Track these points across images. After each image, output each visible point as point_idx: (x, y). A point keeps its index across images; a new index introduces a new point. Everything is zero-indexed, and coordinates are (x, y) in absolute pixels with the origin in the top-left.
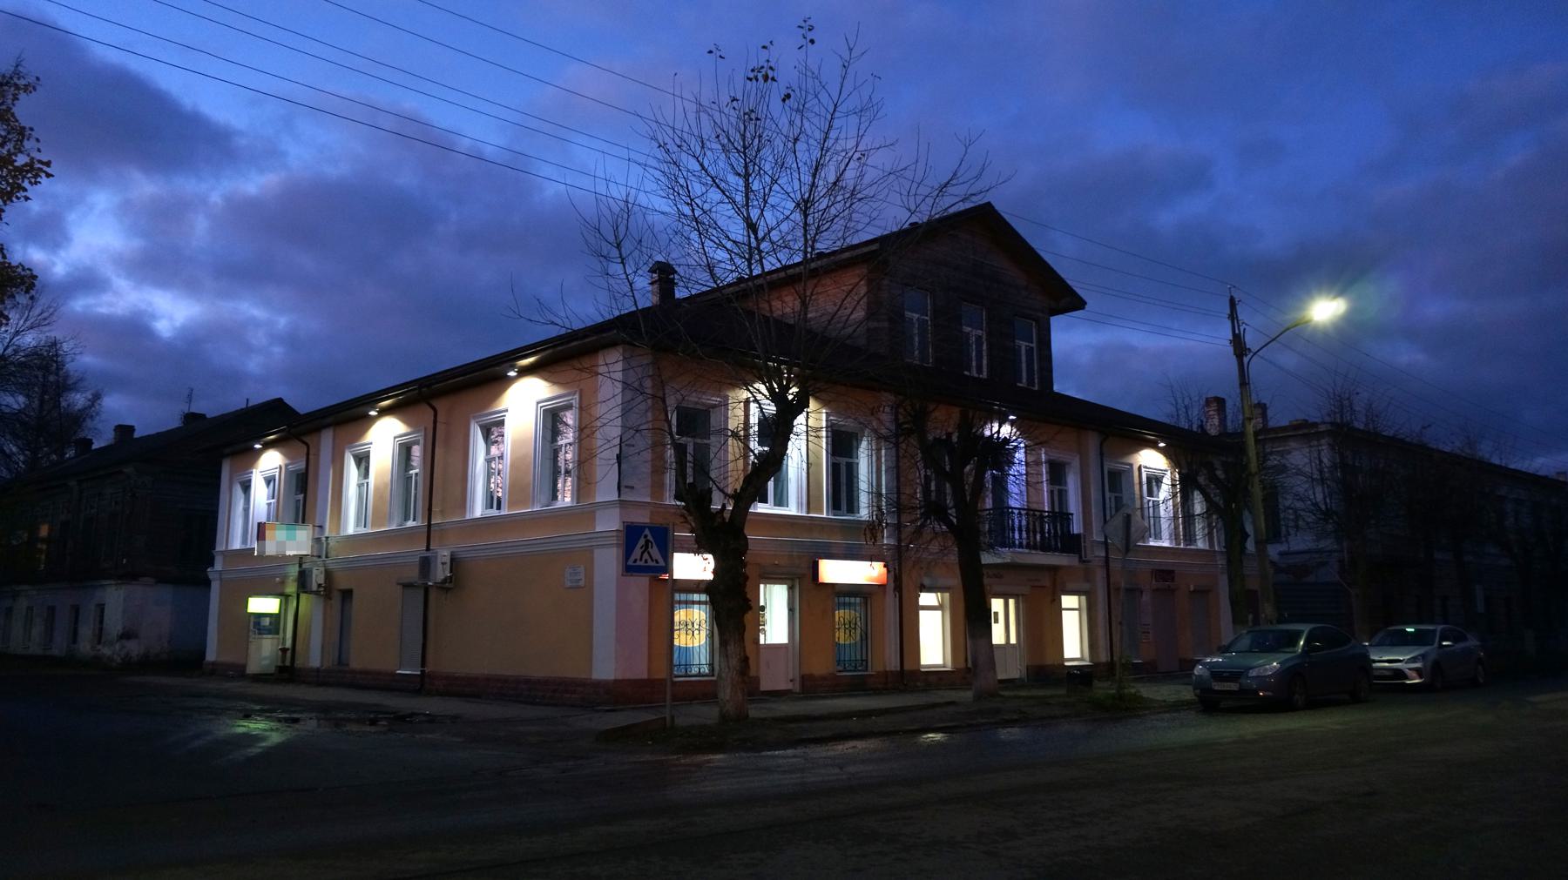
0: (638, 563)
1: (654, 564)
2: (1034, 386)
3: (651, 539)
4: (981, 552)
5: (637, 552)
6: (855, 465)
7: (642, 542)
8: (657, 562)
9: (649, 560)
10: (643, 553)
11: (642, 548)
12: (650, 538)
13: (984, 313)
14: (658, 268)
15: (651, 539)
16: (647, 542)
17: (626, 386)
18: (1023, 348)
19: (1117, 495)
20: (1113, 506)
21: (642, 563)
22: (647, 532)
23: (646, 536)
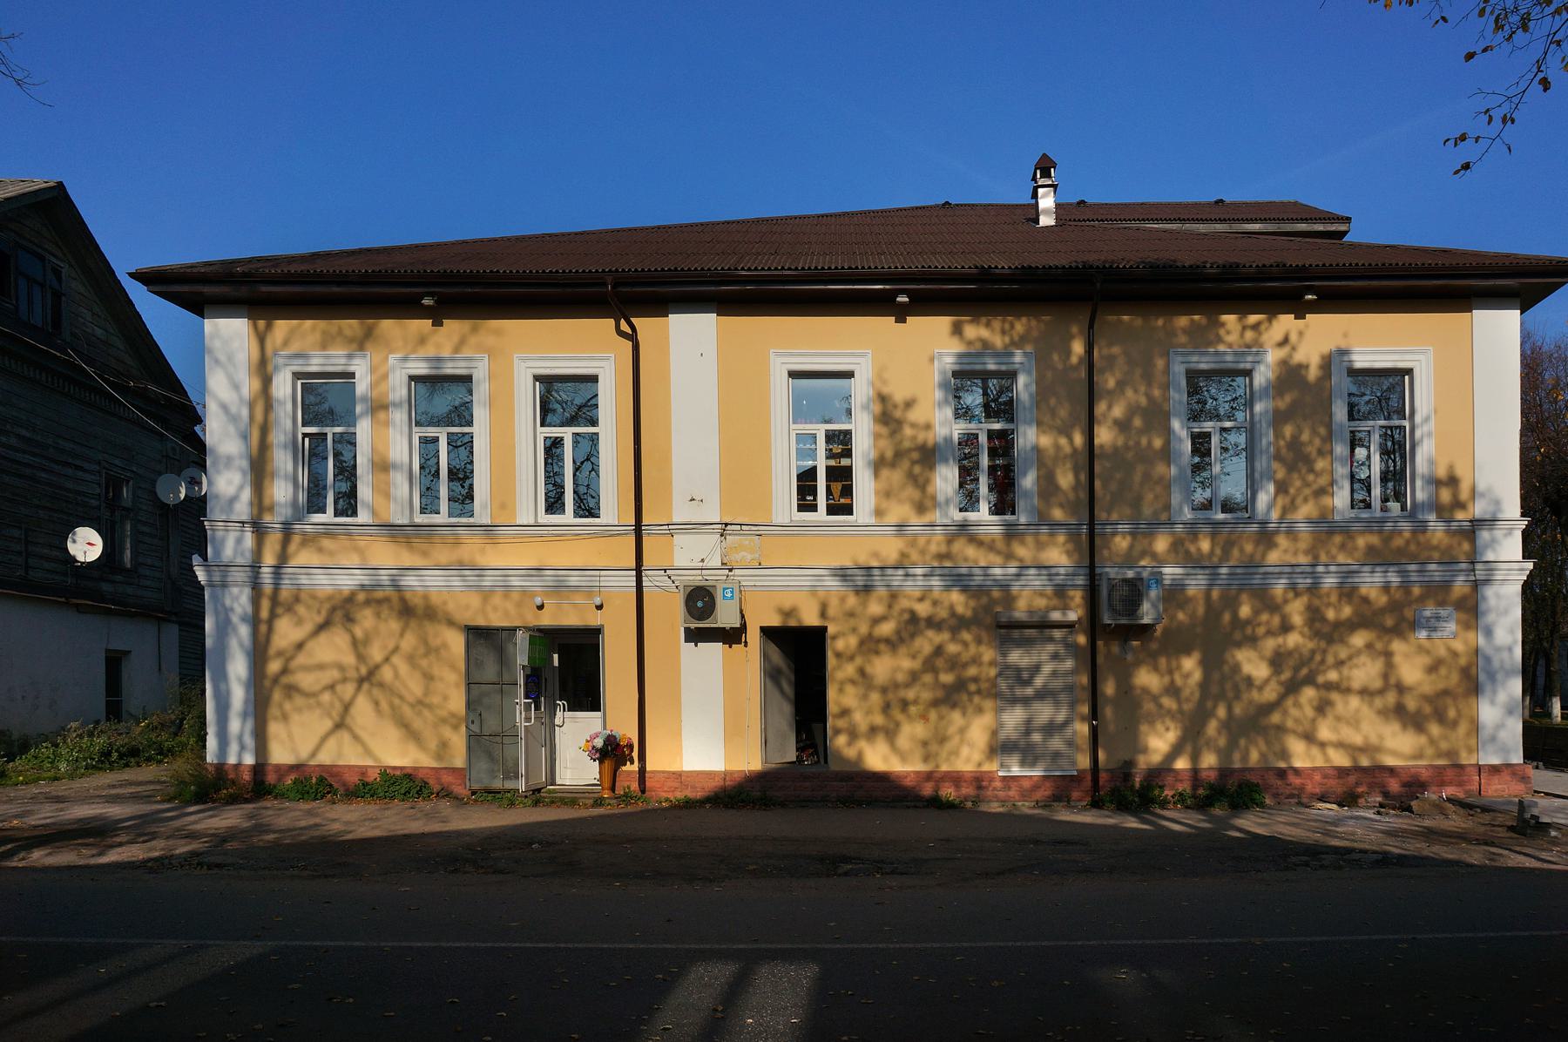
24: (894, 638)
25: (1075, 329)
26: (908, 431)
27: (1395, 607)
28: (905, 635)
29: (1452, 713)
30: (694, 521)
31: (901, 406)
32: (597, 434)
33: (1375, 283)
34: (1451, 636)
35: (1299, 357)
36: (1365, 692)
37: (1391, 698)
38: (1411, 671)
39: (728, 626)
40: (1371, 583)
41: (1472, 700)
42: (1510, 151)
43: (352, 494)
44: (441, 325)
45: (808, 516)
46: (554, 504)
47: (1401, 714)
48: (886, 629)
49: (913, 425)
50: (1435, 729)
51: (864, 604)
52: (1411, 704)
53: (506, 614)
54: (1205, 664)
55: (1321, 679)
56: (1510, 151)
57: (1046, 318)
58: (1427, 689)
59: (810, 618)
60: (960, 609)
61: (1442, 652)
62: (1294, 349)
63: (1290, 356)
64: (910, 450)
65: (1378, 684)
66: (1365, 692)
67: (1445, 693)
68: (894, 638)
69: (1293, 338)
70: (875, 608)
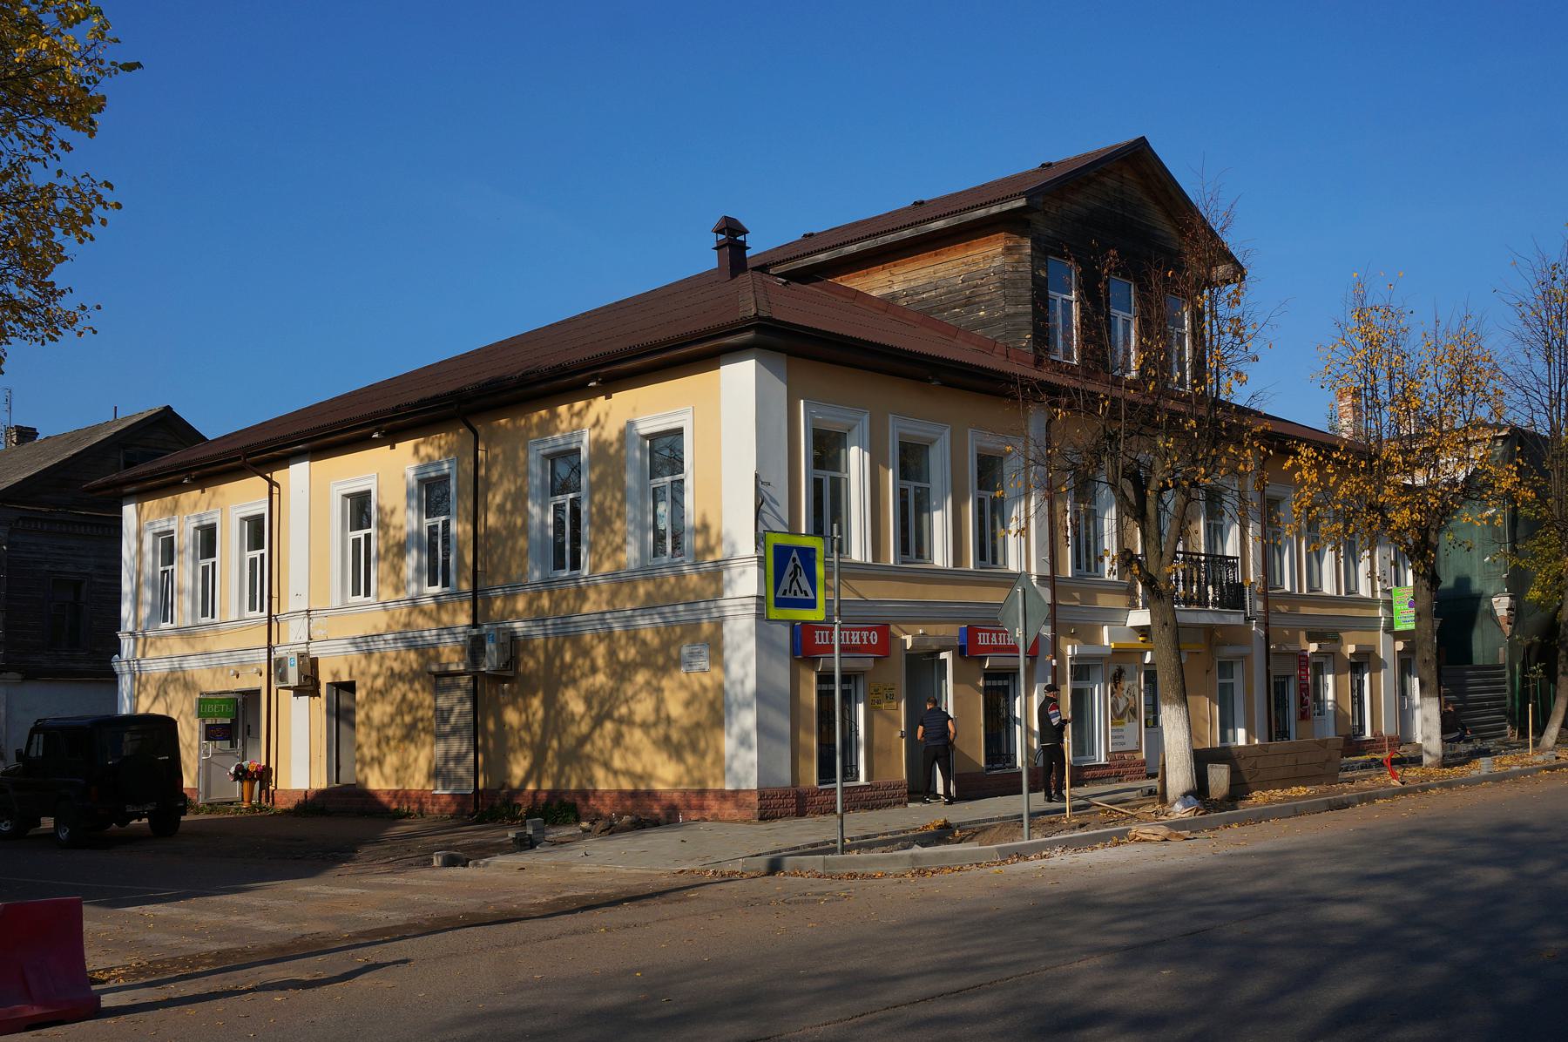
0: (788, 595)
1: (802, 596)
2: (1072, 359)
3: (800, 565)
4: (283, 804)
5: (786, 579)
6: (843, 481)
7: (790, 567)
8: (806, 595)
9: (798, 592)
10: (792, 581)
11: (790, 576)
12: (798, 562)
13: (1330, 695)
14: (727, 228)
15: (800, 565)
16: (796, 567)
17: (1406, 751)
18: (1059, 301)
19: (918, 484)
20: (1557, 382)
21: (791, 596)
22: (795, 554)
23: (794, 560)
24: (383, 689)
26: (392, 532)
27: (665, 646)
29: (702, 744)
31: (389, 513)
34: (701, 675)
35: (605, 435)
36: (645, 726)
41: (717, 731)
45: (358, 599)
52: (675, 735)
58: (686, 722)
60: (415, 666)
63: (600, 435)
65: (652, 718)
66: (645, 726)
67: (698, 725)
69: (602, 418)
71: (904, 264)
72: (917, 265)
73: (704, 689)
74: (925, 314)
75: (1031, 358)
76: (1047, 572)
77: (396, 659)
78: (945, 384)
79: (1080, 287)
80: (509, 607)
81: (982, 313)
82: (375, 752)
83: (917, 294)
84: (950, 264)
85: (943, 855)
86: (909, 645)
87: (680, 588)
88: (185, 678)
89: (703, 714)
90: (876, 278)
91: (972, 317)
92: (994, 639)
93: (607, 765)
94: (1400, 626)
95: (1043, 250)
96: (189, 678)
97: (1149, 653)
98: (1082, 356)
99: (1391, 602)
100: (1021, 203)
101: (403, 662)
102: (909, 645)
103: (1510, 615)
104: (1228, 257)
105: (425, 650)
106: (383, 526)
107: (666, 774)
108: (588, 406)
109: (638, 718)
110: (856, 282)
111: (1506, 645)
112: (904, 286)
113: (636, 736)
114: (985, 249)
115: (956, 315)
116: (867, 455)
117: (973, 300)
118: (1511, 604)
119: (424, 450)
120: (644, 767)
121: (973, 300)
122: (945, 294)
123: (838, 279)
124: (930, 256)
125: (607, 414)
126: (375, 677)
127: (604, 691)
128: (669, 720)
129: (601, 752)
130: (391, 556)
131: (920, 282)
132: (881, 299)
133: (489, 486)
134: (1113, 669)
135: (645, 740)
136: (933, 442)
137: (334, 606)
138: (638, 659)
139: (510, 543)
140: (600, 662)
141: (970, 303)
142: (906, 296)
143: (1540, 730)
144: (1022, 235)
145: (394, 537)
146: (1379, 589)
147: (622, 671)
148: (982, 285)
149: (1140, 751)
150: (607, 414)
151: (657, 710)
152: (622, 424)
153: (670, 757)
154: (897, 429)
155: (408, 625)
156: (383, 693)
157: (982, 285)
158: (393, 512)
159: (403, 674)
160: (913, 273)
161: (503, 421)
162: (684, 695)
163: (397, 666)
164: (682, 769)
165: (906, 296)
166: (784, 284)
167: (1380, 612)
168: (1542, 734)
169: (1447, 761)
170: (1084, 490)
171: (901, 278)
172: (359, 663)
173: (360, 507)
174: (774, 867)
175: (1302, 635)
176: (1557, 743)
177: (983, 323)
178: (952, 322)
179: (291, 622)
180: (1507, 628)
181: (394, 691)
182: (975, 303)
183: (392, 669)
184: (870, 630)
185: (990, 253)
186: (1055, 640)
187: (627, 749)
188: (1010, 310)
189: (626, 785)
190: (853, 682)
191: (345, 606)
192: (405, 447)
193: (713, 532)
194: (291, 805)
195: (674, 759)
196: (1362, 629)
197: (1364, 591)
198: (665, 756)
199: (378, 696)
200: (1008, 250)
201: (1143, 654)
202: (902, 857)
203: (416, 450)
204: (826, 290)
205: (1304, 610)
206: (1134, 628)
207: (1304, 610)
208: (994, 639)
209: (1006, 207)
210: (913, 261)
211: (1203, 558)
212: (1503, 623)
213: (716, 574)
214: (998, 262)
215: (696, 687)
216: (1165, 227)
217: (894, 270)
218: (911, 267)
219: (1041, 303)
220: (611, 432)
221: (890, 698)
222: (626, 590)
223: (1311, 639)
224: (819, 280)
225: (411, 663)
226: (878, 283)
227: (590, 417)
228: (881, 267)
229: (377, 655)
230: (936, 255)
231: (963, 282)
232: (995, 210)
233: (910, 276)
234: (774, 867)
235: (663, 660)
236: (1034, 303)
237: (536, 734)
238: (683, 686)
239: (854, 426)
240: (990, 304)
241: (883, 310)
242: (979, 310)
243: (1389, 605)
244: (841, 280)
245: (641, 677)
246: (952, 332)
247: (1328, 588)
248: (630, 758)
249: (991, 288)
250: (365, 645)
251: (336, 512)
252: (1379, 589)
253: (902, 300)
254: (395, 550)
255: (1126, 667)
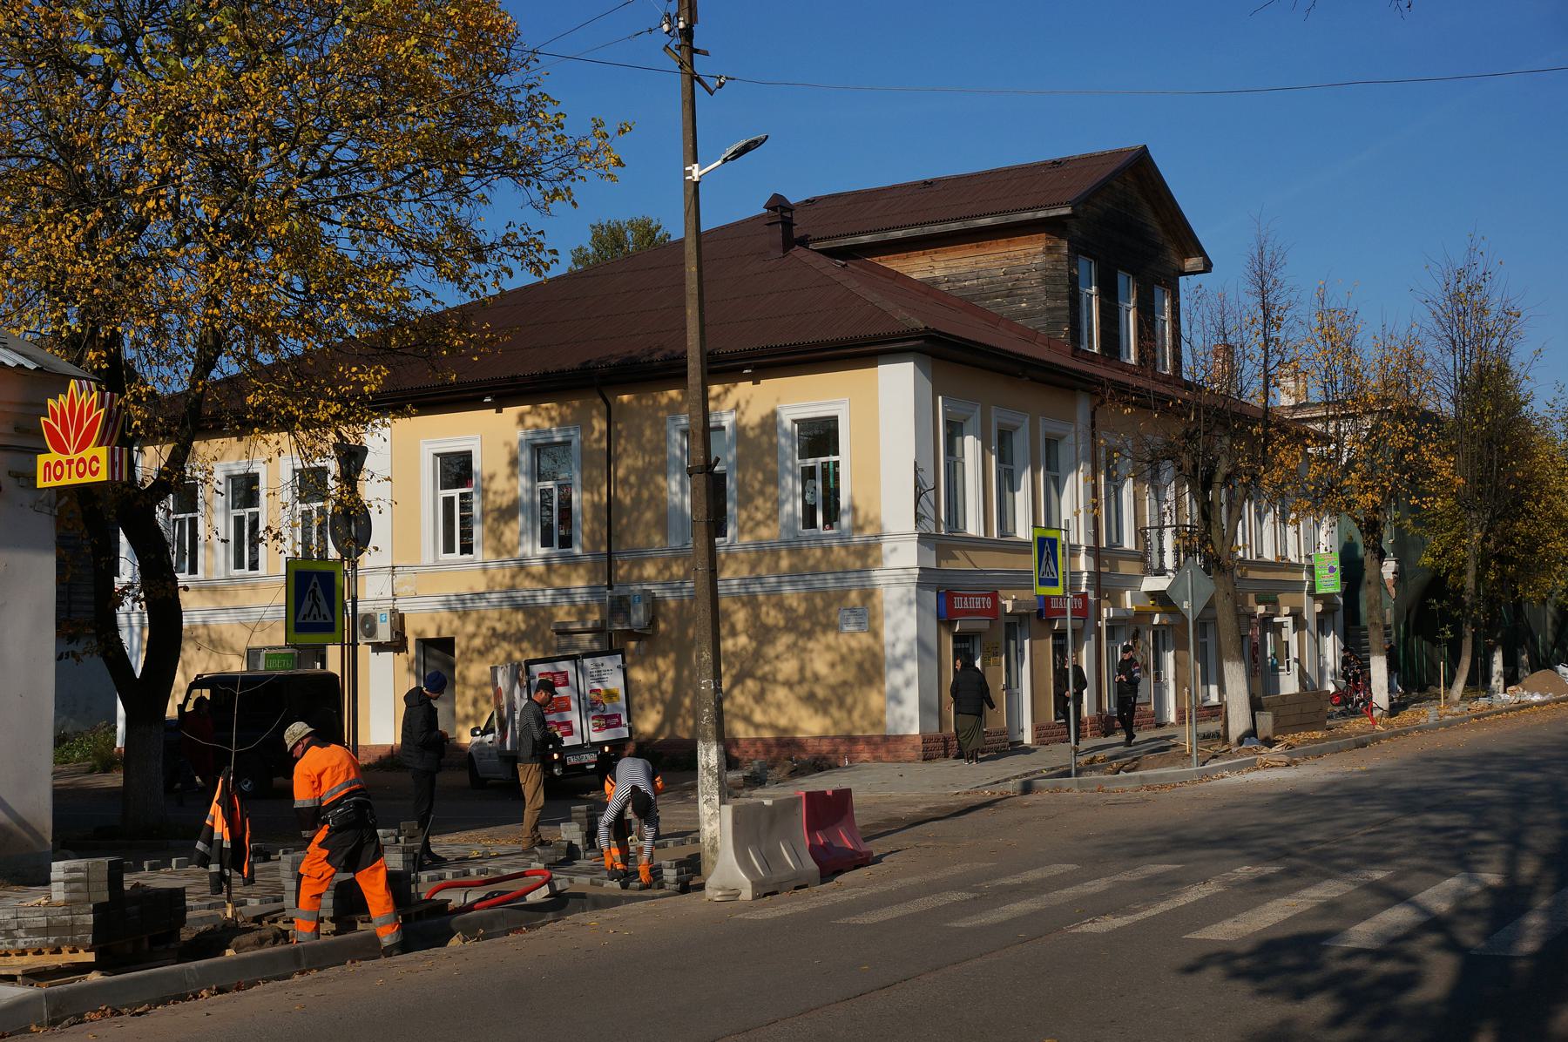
5: (1044, 563)
18: (1084, 295)
24: (483, 648)
25: (595, 412)
26: (491, 496)
27: (811, 613)
28: (513, 639)
29: (849, 700)
30: (375, 565)
31: (487, 478)
32: (258, 513)
33: (808, 355)
34: (852, 639)
35: (744, 421)
36: (788, 684)
37: (803, 690)
38: (820, 665)
39: (383, 641)
40: (792, 595)
41: (865, 689)
42: (755, 144)
43: (467, 533)
44: (242, 440)
45: (449, 556)
46: (449, 548)
47: (810, 699)
48: (477, 642)
49: (495, 493)
50: (834, 711)
51: (464, 624)
52: (821, 692)
53: (262, 642)
54: (679, 665)
55: (759, 673)
56: (755, 144)
57: (576, 403)
58: (832, 680)
59: (445, 633)
60: (523, 626)
61: (844, 650)
62: (743, 413)
63: (740, 419)
64: (492, 511)
65: (796, 677)
66: (788, 684)
67: (845, 683)
68: (483, 648)
69: (743, 405)
70: (470, 628)
71: (945, 252)
72: (959, 254)
73: (851, 650)
74: (966, 303)
75: (1069, 348)
76: (1091, 544)
77: (500, 620)
78: (1033, 379)
79: (1099, 285)
80: (636, 572)
81: (1024, 305)
82: (471, 710)
83: (959, 281)
84: (992, 257)
85: (1161, 776)
86: (1009, 609)
87: (828, 562)
88: (209, 636)
89: (850, 675)
90: (916, 262)
91: (1014, 307)
92: (966, 603)
93: (748, 720)
94: (1321, 590)
95: (1076, 251)
96: (213, 636)
97: (1157, 615)
98: (1102, 347)
99: (1313, 567)
100: (1066, 211)
101: (508, 623)
102: (1009, 609)
103: (1395, 578)
104: (1201, 252)
105: (529, 609)
106: (484, 492)
107: (811, 725)
108: (727, 391)
109: (780, 677)
110: (896, 264)
111: (1392, 606)
112: (944, 273)
113: (781, 693)
114: (1027, 246)
115: (998, 304)
116: (979, 443)
117: (1015, 292)
118: (1396, 568)
119: (529, 421)
120: (790, 719)
121: (1015, 292)
122: (988, 284)
123: (876, 259)
124: (971, 247)
125: (748, 402)
126: (474, 636)
127: (747, 651)
128: (817, 678)
129: (742, 707)
130: (489, 520)
131: (962, 270)
132: (921, 283)
133: (619, 457)
134: (1133, 630)
135: (791, 696)
136: (1017, 428)
137: (425, 563)
138: (782, 623)
139: (635, 514)
140: (740, 626)
141: (1010, 294)
142: (948, 281)
143: (1449, 684)
144: (1061, 237)
145: (494, 502)
146: (1303, 555)
147: (763, 634)
148: (1024, 279)
149: (1150, 703)
150: (748, 402)
151: (802, 669)
152: (766, 411)
153: (816, 711)
154: (997, 417)
155: (513, 588)
156: (482, 653)
157: (1024, 279)
158: (492, 477)
159: (508, 634)
160: (956, 261)
161: (625, 398)
162: (829, 657)
163: (500, 627)
164: (828, 722)
165: (948, 281)
166: (843, 266)
167: (1304, 576)
168: (1450, 688)
169: (1395, 709)
170: (1156, 475)
171: (943, 265)
172: (451, 622)
173: (456, 469)
174: (1027, 788)
175: (1251, 597)
176: (1462, 696)
177: (1026, 314)
178: (994, 310)
179: (367, 577)
180: (1393, 591)
181: (497, 651)
182: (1017, 295)
183: (494, 629)
184: (986, 596)
185: (1031, 251)
186: (1098, 604)
187: (769, 705)
188: (1050, 304)
189: (767, 734)
190: (971, 640)
191: (437, 563)
192: (511, 412)
193: (861, 513)
194: (371, 760)
195: (820, 713)
196: (1293, 591)
197: (1292, 558)
198: (811, 711)
199: (475, 656)
200: (1049, 250)
201: (1152, 616)
202: (1134, 777)
203: (521, 419)
204: (865, 269)
205: (1252, 574)
206: (1147, 593)
207: (1252, 574)
208: (966, 603)
209: (1053, 213)
210: (955, 250)
211: (1188, 529)
212: (1389, 586)
213: (868, 552)
214: (1039, 260)
215: (844, 650)
216: (1154, 224)
217: (935, 256)
218: (951, 255)
219: (1075, 299)
220: (753, 417)
221: (996, 654)
222: (767, 560)
223: (1259, 603)
224: (856, 258)
225: (518, 623)
226: (919, 267)
227: (730, 401)
228: (921, 252)
229: (474, 615)
230: (978, 247)
231: (1005, 274)
232: (1041, 214)
233: (951, 264)
234: (1027, 788)
235: (808, 625)
236: (1070, 298)
237: (666, 692)
238: (829, 648)
239: (969, 418)
240: (1032, 298)
241: (923, 293)
242: (1021, 302)
243: (1311, 570)
244: (880, 261)
245: (785, 640)
246: (995, 320)
247: (1269, 555)
248: (773, 712)
249: (1034, 283)
250: (461, 606)
251: (428, 472)
252: (1303, 555)
253: (944, 286)
254: (495, 514)
255: (1140, 626)
